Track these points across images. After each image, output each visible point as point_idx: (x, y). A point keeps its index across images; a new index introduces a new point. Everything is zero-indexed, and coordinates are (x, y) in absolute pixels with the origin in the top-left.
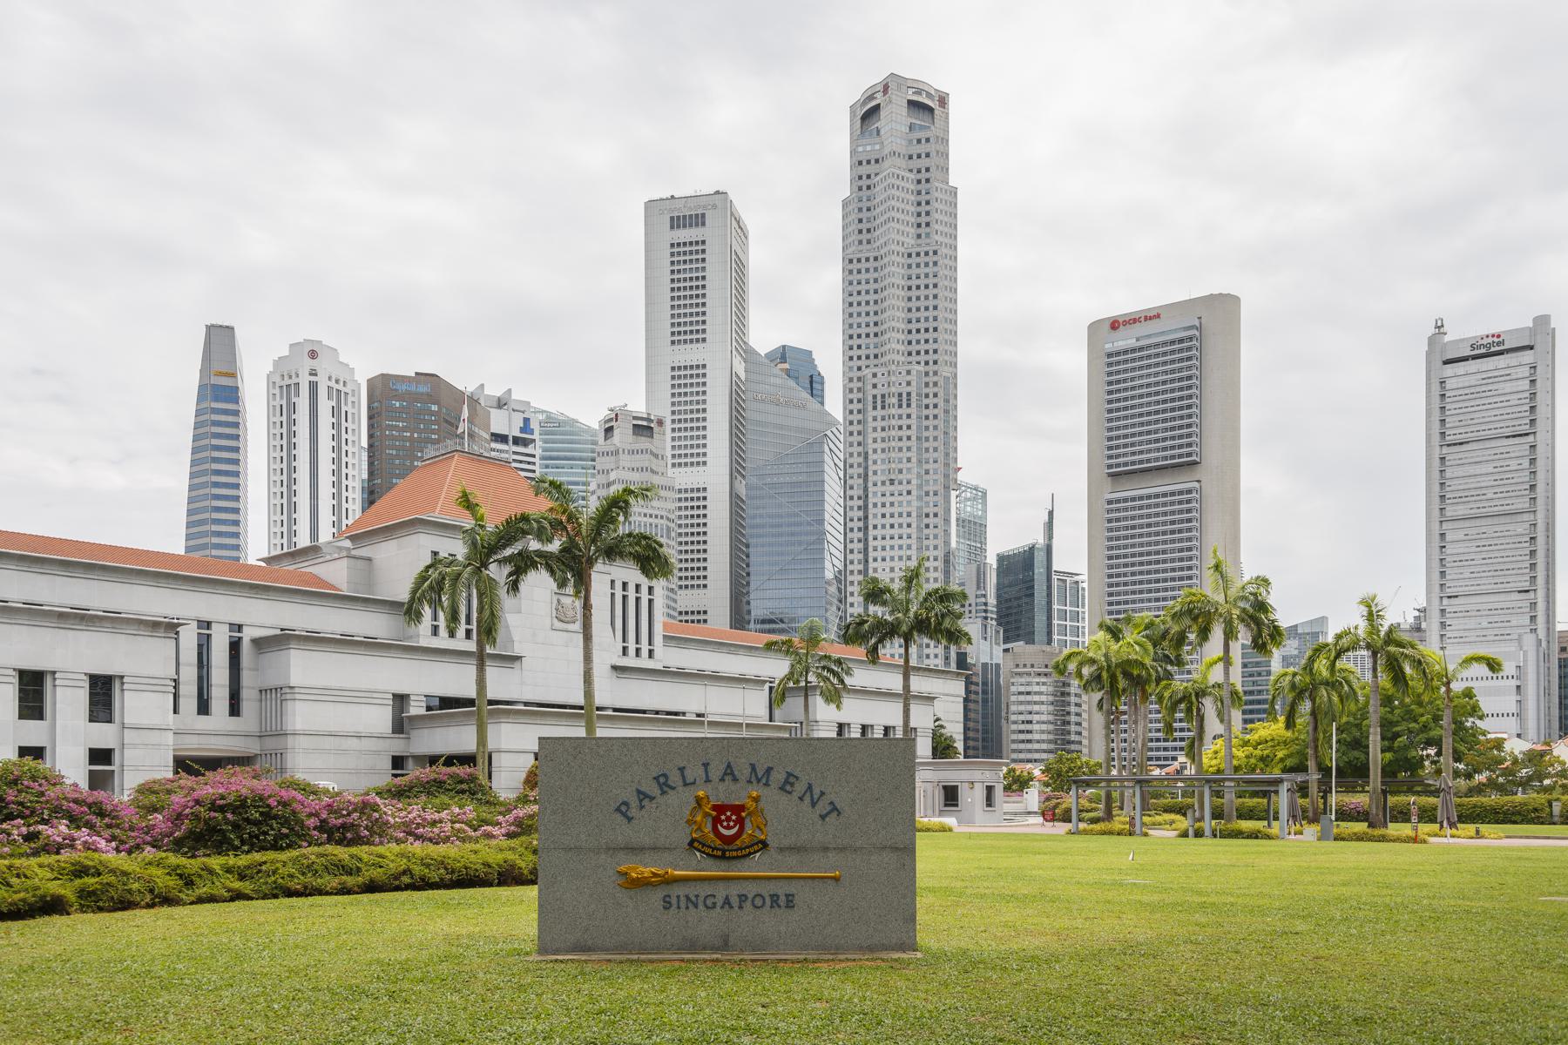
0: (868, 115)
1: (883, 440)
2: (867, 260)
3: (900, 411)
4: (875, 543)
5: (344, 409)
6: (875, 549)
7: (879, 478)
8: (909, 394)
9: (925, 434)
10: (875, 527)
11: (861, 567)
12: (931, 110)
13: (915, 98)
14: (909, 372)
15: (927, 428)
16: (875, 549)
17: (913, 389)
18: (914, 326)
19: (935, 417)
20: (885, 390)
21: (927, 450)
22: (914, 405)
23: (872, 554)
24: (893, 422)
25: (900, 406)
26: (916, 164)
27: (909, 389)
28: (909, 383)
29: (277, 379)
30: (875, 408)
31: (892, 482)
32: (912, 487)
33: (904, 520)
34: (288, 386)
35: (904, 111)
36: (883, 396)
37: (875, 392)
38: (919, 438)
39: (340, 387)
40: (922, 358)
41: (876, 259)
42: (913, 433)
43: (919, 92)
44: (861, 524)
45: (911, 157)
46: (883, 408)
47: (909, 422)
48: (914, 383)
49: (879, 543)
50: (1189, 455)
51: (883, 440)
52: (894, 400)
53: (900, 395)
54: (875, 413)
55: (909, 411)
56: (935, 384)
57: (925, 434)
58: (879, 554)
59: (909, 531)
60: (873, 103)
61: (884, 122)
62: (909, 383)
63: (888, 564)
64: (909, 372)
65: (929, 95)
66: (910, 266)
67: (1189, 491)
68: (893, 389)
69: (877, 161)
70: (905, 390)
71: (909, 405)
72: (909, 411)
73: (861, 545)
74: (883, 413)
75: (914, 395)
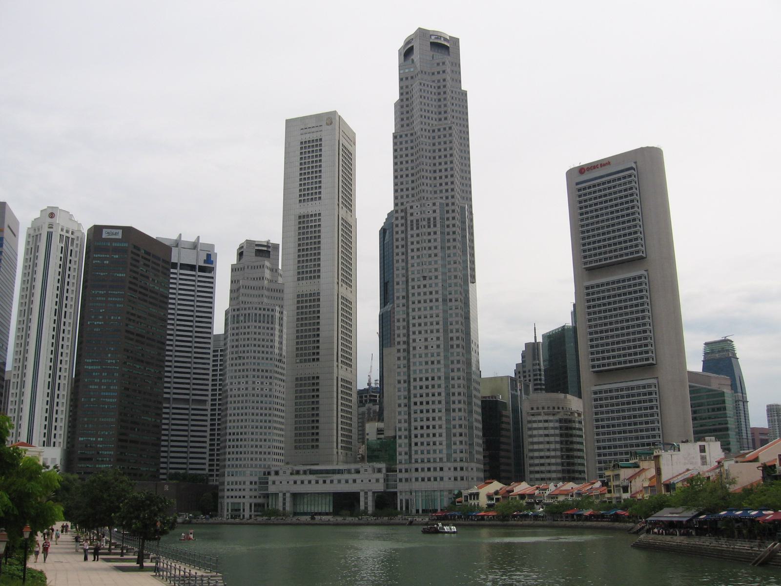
0: (407, 53)
1: (418, 242)
2: (406, 135)
3: (429, 230)
4: (414, 321)
5: (70, 248)
6: (413, 288)
7: (416, 276)
8: (435, 218)
9: (447, 245)
10: (416, 436)
11: (405, 339)
12: (447, 48)
13: (436, 41)
14: (434, 204)
15: (449, 241)
16: (413, 288)
17: (437, 215)
18: (437, 147)
19: (454, 233)
20: (419, 216)
21: (452, 339)
22: (438, 225)
23: (412, 329)
24: (425, 245)
25: (429, 227)
26: (437, 77)
27: (434, 215)
28: (434, 211)
29: (32, 232)
30: (412, 229)
31: (425, 278)
32: (439, 273)
33: (435, 319)
34: (37, 236)
35: (429, 48)
36: (417, 221)
37: (412, 218)
38: (442, 233)
39: (69, 235)
40: (444, 195)
41: (412, 134)
42: (438, 244)
43: (439, 37)
44: (407, 433)
45: (433, 74)
46: (418, 228)
47: (439, 390)
48: (438, 211)
49: (416, 306)
50: (647, 359)
51: (418, 242)
52: (425, 223)
53: (429, 219)
54: (412, 232)
55: (435, 229)
56: (453, 211)
57: (447, 245)
58: (417, 329)
59: (437, 327)
60: (409, 46)
61: (416, 56)
62: (434, 211)
63: (424, 335)
64: (434, 204)
65: (445, 39)
66: (435, 172)
67: (640, 277)
68: (424, 216)
69: (412, 78)
70: (432, 215)
71: (435, 226)
72: (435, 229)
73: (405, 331)
74: (418, 232)
75: (438, 219)
